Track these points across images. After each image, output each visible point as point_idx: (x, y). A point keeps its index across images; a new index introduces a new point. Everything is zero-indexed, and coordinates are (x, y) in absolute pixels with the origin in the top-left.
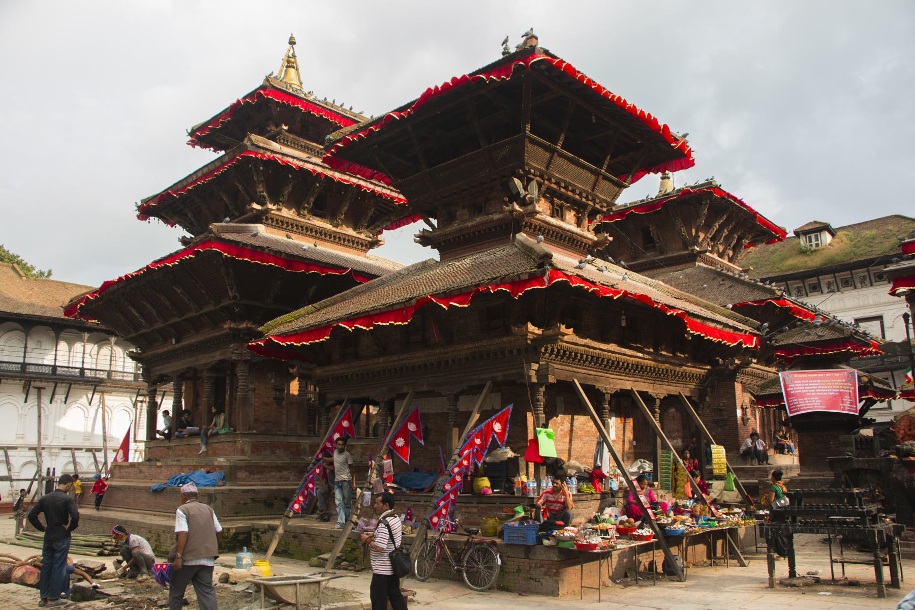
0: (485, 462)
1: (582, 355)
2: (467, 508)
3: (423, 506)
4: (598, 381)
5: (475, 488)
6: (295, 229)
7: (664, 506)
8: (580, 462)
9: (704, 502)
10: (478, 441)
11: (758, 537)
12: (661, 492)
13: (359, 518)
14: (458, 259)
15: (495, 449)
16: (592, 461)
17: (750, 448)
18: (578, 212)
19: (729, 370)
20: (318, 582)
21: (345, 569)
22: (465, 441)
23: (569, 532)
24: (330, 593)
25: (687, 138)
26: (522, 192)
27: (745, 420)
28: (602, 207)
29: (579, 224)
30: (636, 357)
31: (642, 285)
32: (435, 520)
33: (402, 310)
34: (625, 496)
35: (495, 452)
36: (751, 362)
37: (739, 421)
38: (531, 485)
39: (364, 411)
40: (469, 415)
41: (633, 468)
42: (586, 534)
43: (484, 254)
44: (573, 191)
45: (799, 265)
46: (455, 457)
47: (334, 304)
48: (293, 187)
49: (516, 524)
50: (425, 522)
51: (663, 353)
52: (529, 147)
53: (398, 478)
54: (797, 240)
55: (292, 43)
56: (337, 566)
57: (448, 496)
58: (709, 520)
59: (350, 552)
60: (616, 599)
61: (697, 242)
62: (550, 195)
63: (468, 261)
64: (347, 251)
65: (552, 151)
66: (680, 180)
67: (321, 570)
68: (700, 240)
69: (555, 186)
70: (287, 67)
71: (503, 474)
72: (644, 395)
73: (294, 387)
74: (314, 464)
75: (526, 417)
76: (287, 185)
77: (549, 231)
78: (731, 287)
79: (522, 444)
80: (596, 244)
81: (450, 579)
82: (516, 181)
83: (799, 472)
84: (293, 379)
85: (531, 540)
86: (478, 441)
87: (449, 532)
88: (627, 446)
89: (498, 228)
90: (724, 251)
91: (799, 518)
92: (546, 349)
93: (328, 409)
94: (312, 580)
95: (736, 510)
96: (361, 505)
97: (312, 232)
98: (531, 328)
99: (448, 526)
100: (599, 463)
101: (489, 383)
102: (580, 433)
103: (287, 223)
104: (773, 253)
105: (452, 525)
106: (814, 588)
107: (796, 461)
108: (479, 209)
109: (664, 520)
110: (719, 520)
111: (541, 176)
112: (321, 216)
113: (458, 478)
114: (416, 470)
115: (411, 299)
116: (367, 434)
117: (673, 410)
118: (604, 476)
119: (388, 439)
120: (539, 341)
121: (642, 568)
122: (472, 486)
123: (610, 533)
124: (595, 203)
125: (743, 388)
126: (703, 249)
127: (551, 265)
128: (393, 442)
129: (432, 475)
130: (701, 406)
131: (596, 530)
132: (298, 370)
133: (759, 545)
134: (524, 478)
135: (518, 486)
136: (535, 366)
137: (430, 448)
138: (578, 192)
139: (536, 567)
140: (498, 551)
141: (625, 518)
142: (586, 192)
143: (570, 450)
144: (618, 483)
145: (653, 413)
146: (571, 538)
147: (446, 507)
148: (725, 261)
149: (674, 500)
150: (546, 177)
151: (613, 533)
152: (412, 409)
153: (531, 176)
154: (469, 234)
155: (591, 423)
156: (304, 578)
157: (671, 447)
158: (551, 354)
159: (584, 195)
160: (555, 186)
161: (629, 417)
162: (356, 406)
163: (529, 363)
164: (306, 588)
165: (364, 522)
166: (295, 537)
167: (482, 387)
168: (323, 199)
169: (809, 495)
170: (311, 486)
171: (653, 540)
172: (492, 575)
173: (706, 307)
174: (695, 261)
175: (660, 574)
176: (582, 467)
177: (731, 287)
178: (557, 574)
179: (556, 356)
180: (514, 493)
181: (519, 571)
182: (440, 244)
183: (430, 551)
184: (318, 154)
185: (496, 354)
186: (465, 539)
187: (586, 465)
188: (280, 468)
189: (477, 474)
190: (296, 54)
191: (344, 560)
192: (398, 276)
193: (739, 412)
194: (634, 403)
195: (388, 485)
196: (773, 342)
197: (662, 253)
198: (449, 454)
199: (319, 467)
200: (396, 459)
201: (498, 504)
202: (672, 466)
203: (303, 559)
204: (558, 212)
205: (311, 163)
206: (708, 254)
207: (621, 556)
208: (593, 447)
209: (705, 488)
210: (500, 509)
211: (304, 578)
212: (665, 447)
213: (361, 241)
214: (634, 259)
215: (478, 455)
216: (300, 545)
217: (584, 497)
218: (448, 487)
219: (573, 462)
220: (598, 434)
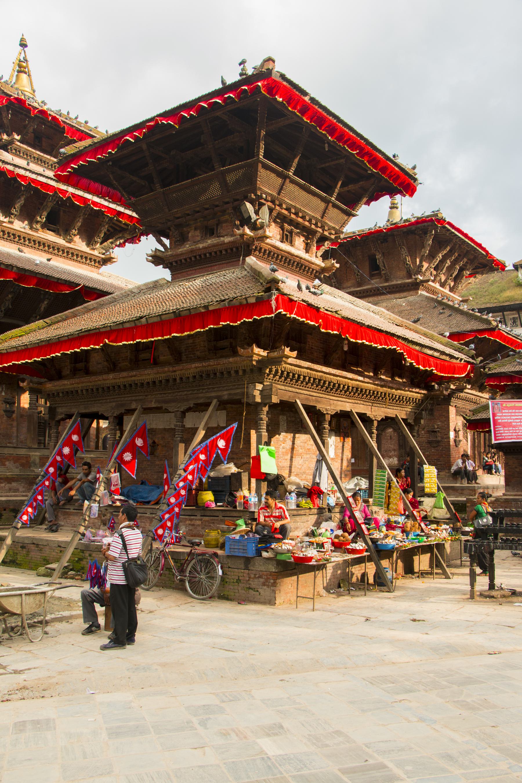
0: (209, 477)
1: (305, 377)
2: (191, 520)
3: (149, 518)
4: (319, 402)
5: (199, 502)
6: (27, 243)
7: (377, 522)
8: (299, 478)
9: (415, 519)
10: (202, 457)
11: (463, 551)
12: (375, 508)
13: (86, 528)
14: (188, 280)
15: (219, 464)
16: (311, 477)
17: (461, 468)
18: (307, 238)
19: (444, 396)
20: (44, 593)
21: (72, 578)
22: (191, 457)
23: (287, 545)
24: (56, 602)
25: (415, 171)
26: (254, 217)
27: (457, 442)
28: (330, 234)
29: (307, 250)
30: (357, 380)
31: (366, 312)
32: (160, 532)
33: (132, 328)
34: (343, 511)
35: (219, 467)
36: (465, 388)
37: (452, 443)
38: (253, 500)
39: (94, 425)
40: (194, 431)
41: (349, 485)
42: (302, 547)
43: (214, 276)
44: (303, 218)
45: (516, 297)
46: (181, 472)
47: (65, 320)
48: (25, 200)
49: (237, 537)
50: (151, 535)
51: (383, 377)
52: (262, 173)
53: (126, 491)
54: (515, 273)
55: (23, 45)
56: (64, 575)
57: (173, 509)
58: (418, 535)
59: (77, 562)
60: (329, 608)
61: (420, 272)
62: (281, 220)
63: (198, 282)
64: (80, 267)
65: (285, 177)
66: (408, 209)
67: (47, 580)
68: (424, 269)
69: (286, 212)
70: (19, 72)
71: (226, 488)
72: (363, 417)
73: (25, 400)
74: (43, 476)
75: (250, 434)
76: (19, 198)
77: (278, 256)
78: (450, 315)
79: (245, 460)
80: (324, 270)
81: (173, 588)
82: (248, 205)
83: (504, 492)
84: (24, 391)
85: (251, 552)
86: (202, 457)
87: (173, 544)
88: (345, 463)
89: (229, 251)
90: (446, 281)
91: (500, 534)
92: (271, 371)
93: (59, 422)
94: (37, 591)
95: (444, 526)
96: (89, 517)
97: (44, 246)
98: (256, 350)
99: (172, 538)
100: (317, 480)
101: (215, 402)
102: (301, 451)
103: (19, 236)
104: (492, 284)
105: (177, 537)
106: (510, 599)
107: (502, 482)
108: (211, 232)
109: (377, 535)
110: (428, 536)
111: (273, 202)
112: (57, 232)
113: (183, 492)
114: (142, 483)
115: (141, 318)
116: (97, 447)
117: (391, 430)
118: (322, 492)
119: (115, 454)
120: (263, 363)
121: (354, 580)
122: (196, 500)
123: (326, 546)
124: (323, 230)
125: (457, 411)
126: (425, 279)
127: (278, 289)
128: (120, 457)
129: (158, 488)
130: (416, 428)
131: (312, 543)
132: (28, 384)
133: (463, 559)
134: (246, 493)
135: (239, 501)
136: (259, 387)
137: (157, 463)
138: (307, 218)
139: (255, 577)
140: (218, 562)
141: (340, 532)
142: (316, 219)
143: (291, 467)
144: (335, 499)
145: (371, 433)
146: (289, 551)
147: (171, 519)
148: (446, 291)
149: (386, 516)
150: (277, 203)
151: (328, 546)
152: (140, 424)
153: (263, 201)
154: (200, 256)
155: (312, 442)
156: (29, 589)
157: (385, 464)
158: (275, 376)
159: (314, 222)
160: (286, 212)
161: (348, 437)
162: (86, 420)
163: (254, 383)
164: (31, 598)
165: (91, 532)
166: (23, 547)
167: (208, 405)
168: (60, 216)
169: (510, 515)
170: (40, 497)
171: (365, 554)
172: (213, 585)
173: (425, 335)
174: (418, 289)
175: (371, 585)
176: (302, 483)
177: (450, 315)
178: (274, 584)
179: (280, 377)
180: (235, 507)
181: (238, 581)
182: (171, 264)
183: (154, 561)
184: (50, 167)
185: (222, 373)
186: (188, 550)
187: (306, 482)
188: (9, 480)
189: (201, 488)
190: (28, 58)
191: (71, 570)
192: (130, 294)
193: (452, 435)
194: (353, 424)
195: (116, 497)
196: (487, 370)
197: (387, 280)
198: (174, 468)
199: (48, 480)
200: (124, 473)
201: (221, 517)
202: (386, 484)
203: (31, 569)
204: (287, 238)
205: (44, 176)
206: (430, 283)
207: (335, 568)
208: (313, 465)
209: (416, 504)
210: (223, 522)
211: (29, 589)
212: (381, 466)
213: (94, 258)
214: (359, 285)
215: (203, 471)
216: (28, 555)
217: (302, 512)
218: (173, 500)
219: (293, 478)
220: (318, 452)
